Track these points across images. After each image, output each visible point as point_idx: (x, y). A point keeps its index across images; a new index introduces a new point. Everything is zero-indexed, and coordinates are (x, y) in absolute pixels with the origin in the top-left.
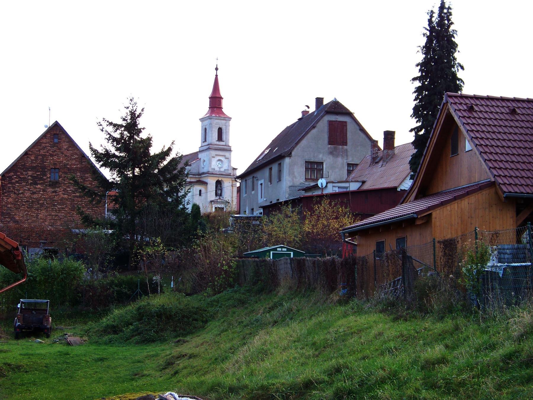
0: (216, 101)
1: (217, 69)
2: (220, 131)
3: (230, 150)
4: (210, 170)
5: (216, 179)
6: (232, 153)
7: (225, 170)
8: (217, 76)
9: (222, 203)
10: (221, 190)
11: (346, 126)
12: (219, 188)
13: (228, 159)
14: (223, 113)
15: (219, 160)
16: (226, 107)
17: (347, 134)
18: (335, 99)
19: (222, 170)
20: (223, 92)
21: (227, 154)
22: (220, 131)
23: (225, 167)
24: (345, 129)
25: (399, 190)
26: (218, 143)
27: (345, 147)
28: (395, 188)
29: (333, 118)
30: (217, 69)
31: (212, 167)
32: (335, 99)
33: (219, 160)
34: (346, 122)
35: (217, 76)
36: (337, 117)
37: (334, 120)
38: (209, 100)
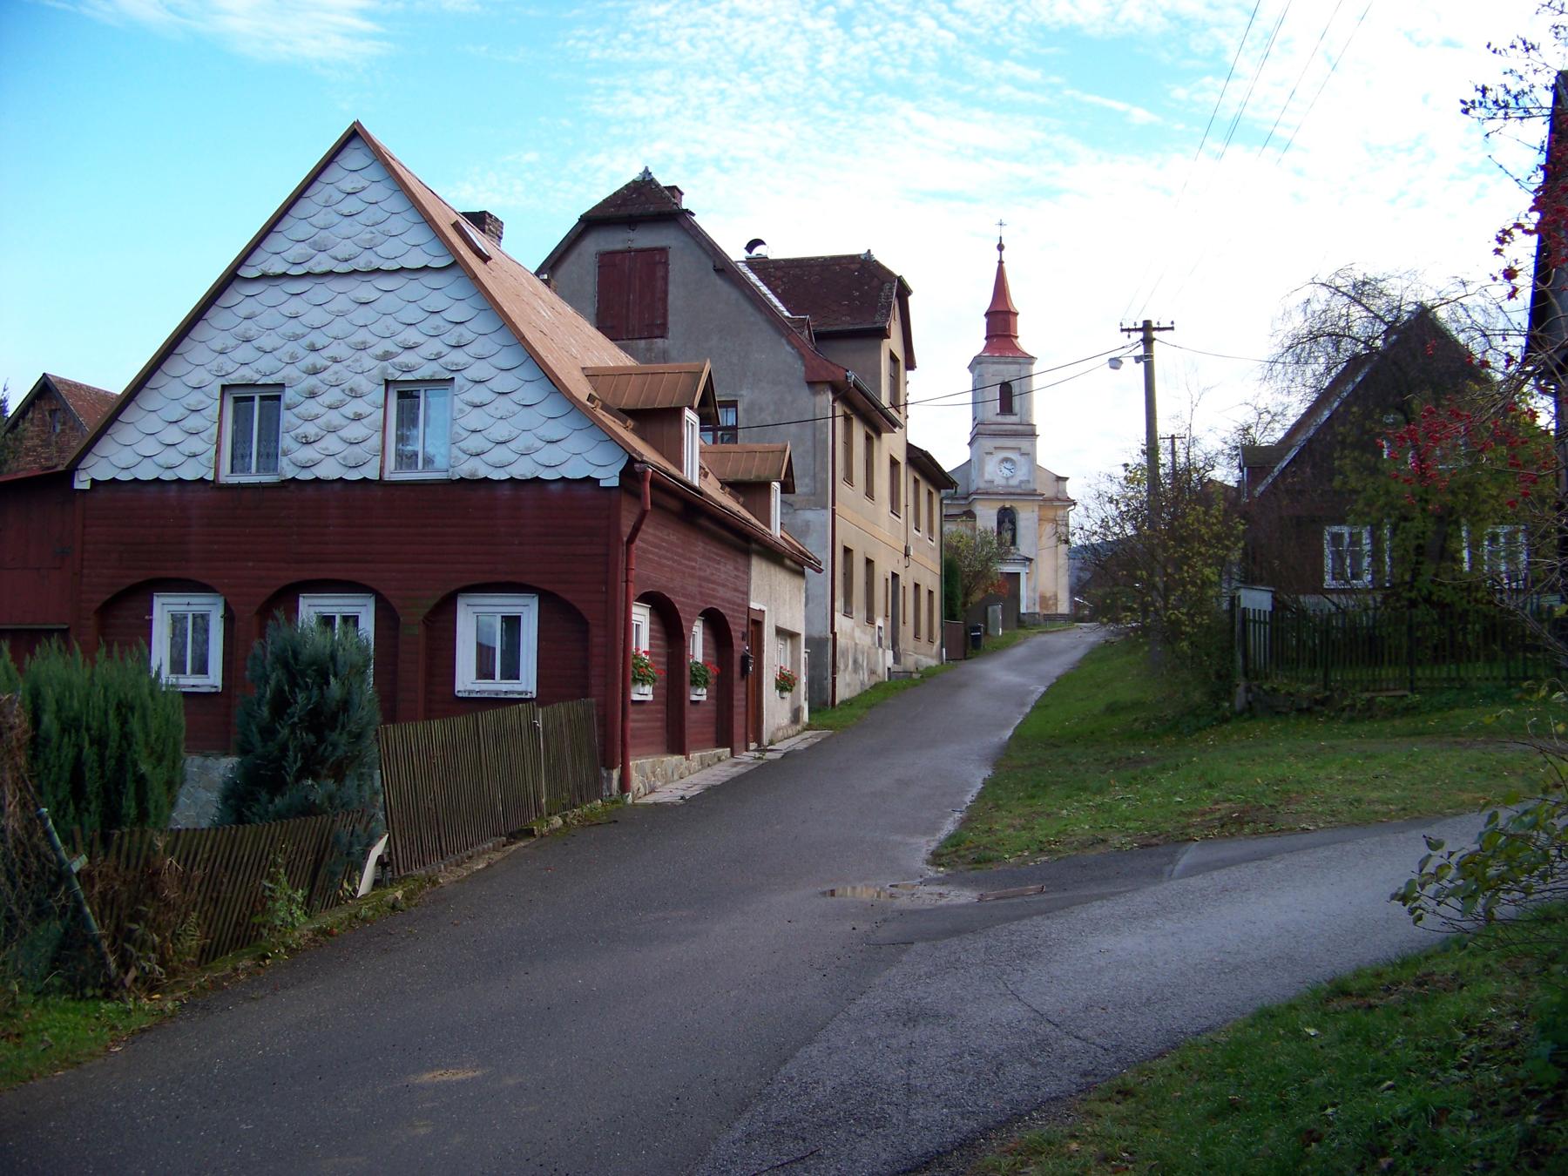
0: (1000, 321)
1: (1001, 247)
2: (1006, 389)
3: (1032, 434)
4: (982, 485)
5: (1000, 505)
6: (1039, 441)
7: (1021, 482)
8: (1001, 262)
9: (1014, 561)
10: (1014, 531)
11: (666, 264)
12: (1007, 525)
13: (1030, 456)
14: (1016, 349)
15: (1006, 460)
16: (1026, 337)
17: (666, 292)
18: (647, 172)
19: (1014, 482)
20: (1018, 298)
21: (1023, 444)
22: (1006, 389)
23: (1021, 474)
24: (660, 274)
25: (82, 482)
26: (1000, 419)
27: (659, 341)
28: (598, 480)
29: (616, 240)
30: (1001, 247)
31: (987, 477)
32: (647, 172)
33: (1006, 460)
34: (663, 251)
35: (1001, 262)
36: (632, 235)
37: (619, 247)
38: (985, 320)
